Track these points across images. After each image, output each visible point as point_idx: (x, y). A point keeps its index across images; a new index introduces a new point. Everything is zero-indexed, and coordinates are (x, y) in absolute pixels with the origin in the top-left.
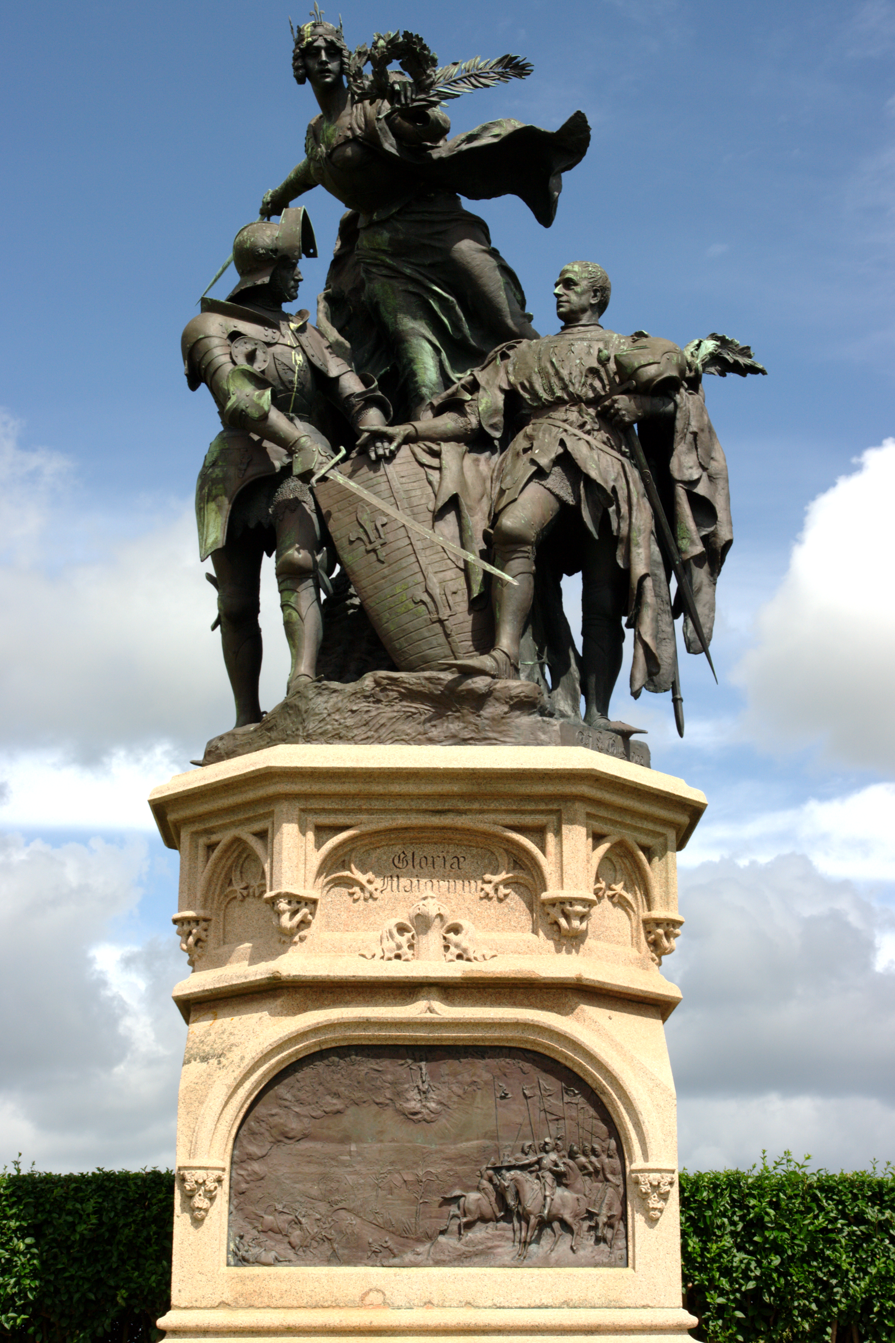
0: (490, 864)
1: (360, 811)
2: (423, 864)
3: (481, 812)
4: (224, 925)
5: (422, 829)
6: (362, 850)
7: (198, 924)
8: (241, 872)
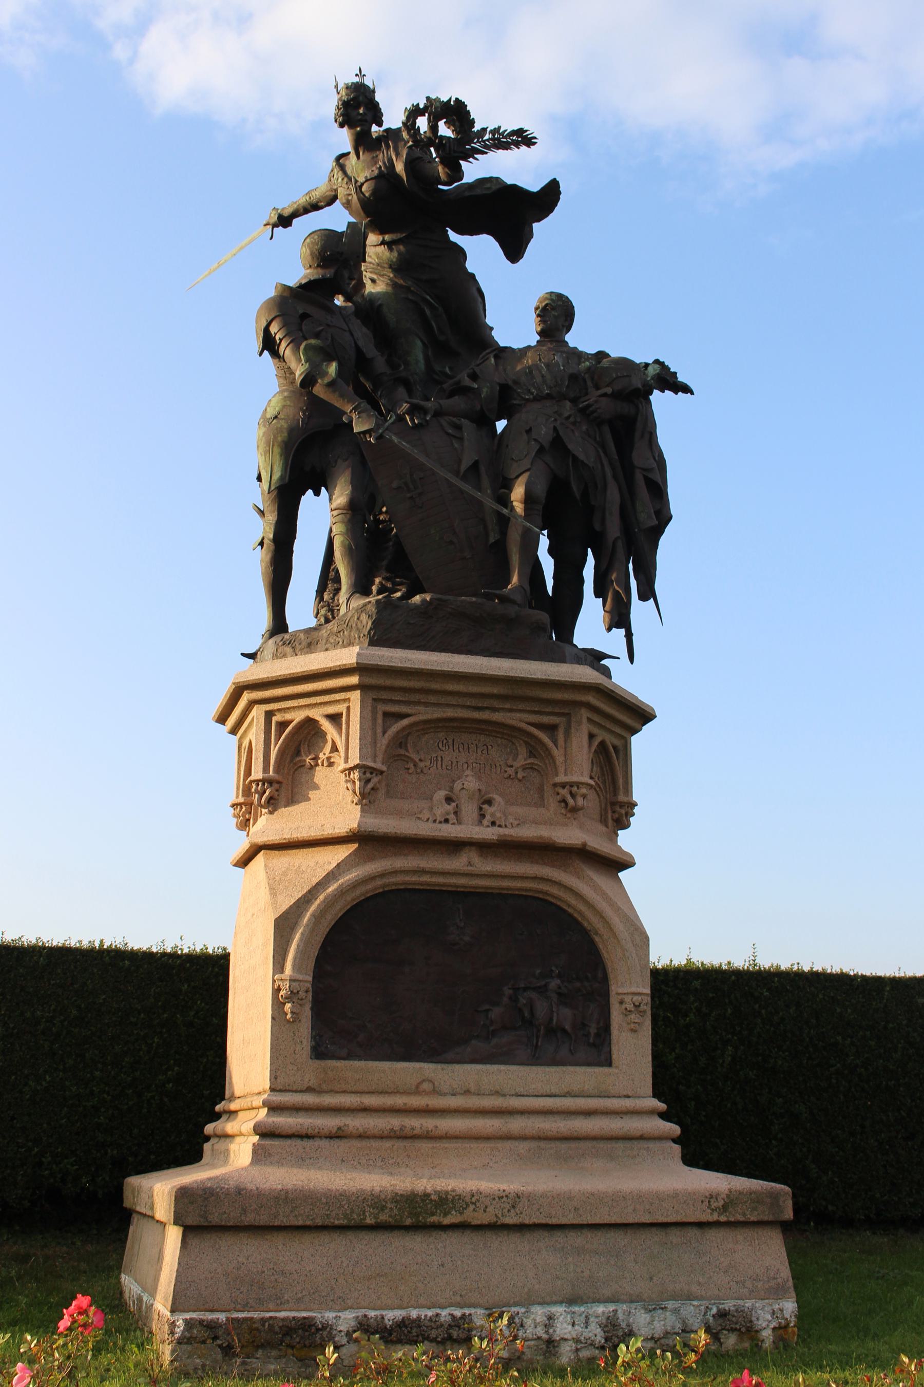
1: (418, 703)
2: (461, 749)
3: (511, 710)
5: (463, 720)
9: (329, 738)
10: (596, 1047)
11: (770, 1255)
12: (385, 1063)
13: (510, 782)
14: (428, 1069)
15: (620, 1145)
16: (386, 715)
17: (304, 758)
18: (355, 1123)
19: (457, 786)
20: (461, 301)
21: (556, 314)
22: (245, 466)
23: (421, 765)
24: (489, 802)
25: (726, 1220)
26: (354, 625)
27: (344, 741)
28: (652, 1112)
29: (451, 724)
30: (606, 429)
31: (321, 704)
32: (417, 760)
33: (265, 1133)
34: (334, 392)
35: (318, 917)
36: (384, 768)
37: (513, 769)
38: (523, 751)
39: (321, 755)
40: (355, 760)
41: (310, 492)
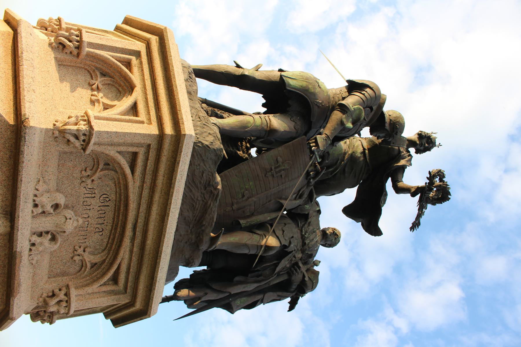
0: (97, 249)
1: (143, 182)
2: (100, 212)
4: (73, 66)
5: (127, 205)
6: (115, 177)
7: (76, 48)
8: (109, 84)
9: (115, 103)
13: (71, 251)
16: (135, 155)
17: (99, 79)
19: (69, 213)
20: (332, 187)
21: (331, 238)
22: (295, 65)
23: (89, 181)
24: (54, 239)
26: (205, 130)
27: (114, 116)
29: (122, 206)
30: (285, 277)
31: (146, 99)
32: (93, 178)
34: (338, 125)
36: (88, 152)
37: (82, 253)
38: (97, 259)
39: (101, 95)
40: (98, 126)
41: (264, 101)
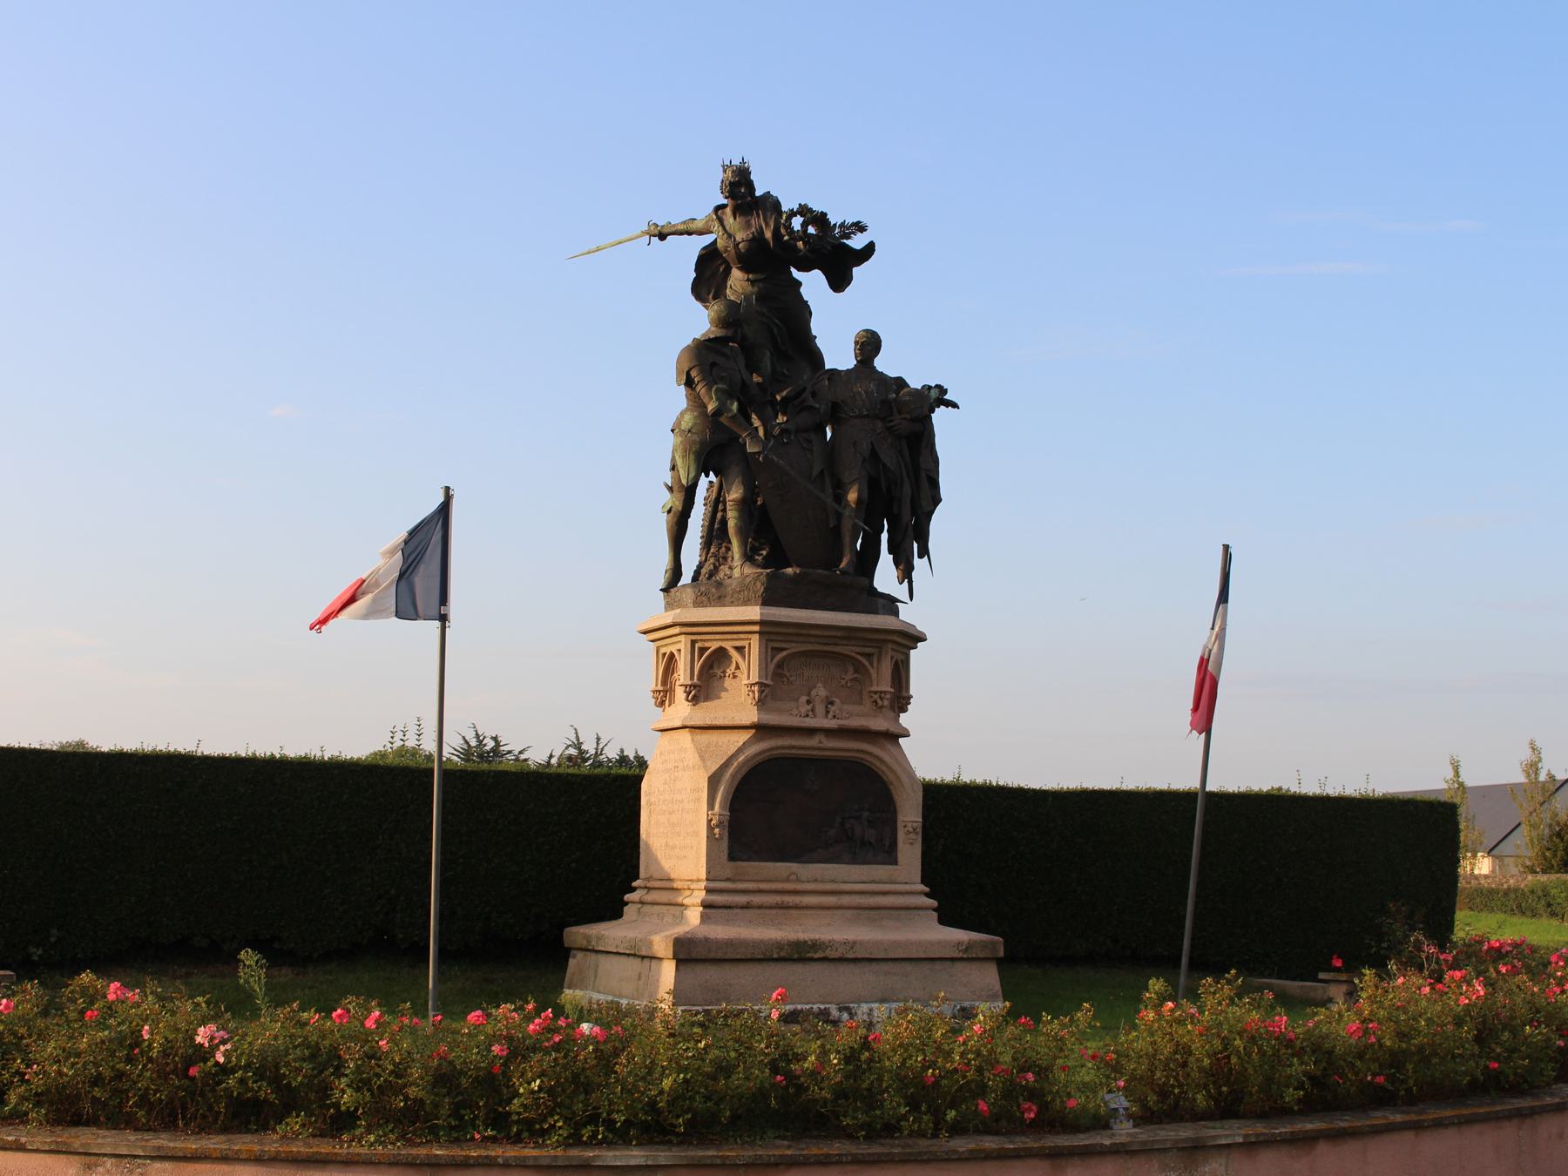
10: (888, 854)
11: (989, 977)
12: (779, 864)
14: (794, 867)
15: (903, 912)
18: (757, 899)
19: (813, 693)
21: (869, 345)
24: (832, 703)
25: (968, 956)
28: (920, 893)
33: (706, 905)
35: (733, 776)
38: (851, 670)
